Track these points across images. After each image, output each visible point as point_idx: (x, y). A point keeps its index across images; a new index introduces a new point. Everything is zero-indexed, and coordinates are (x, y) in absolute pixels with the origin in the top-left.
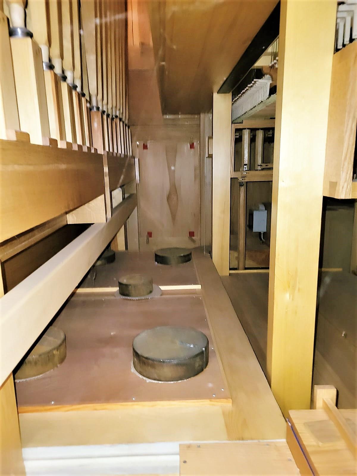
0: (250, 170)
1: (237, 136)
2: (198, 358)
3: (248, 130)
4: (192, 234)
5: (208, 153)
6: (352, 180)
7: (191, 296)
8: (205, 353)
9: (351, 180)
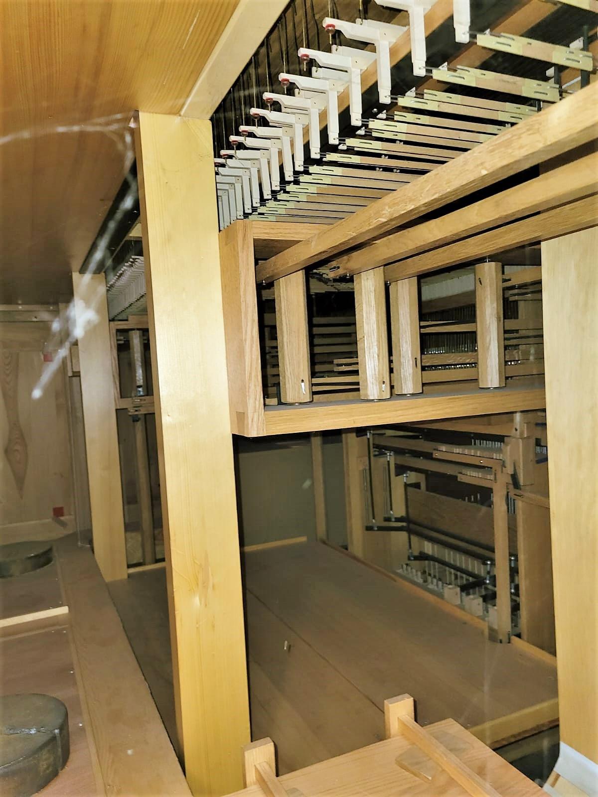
0: (147, 395)
1: (120, 340)
2: (45, 751)
3: (138, 331)
4: (58, 512)
5: (72, 369)
6: (263, 410)
7: (47, 630)
8: (58, 738)
9: (262, 408)
